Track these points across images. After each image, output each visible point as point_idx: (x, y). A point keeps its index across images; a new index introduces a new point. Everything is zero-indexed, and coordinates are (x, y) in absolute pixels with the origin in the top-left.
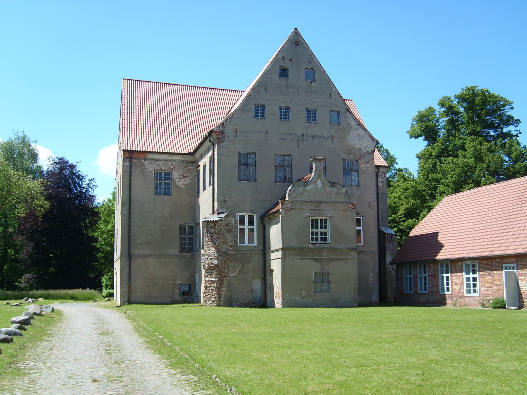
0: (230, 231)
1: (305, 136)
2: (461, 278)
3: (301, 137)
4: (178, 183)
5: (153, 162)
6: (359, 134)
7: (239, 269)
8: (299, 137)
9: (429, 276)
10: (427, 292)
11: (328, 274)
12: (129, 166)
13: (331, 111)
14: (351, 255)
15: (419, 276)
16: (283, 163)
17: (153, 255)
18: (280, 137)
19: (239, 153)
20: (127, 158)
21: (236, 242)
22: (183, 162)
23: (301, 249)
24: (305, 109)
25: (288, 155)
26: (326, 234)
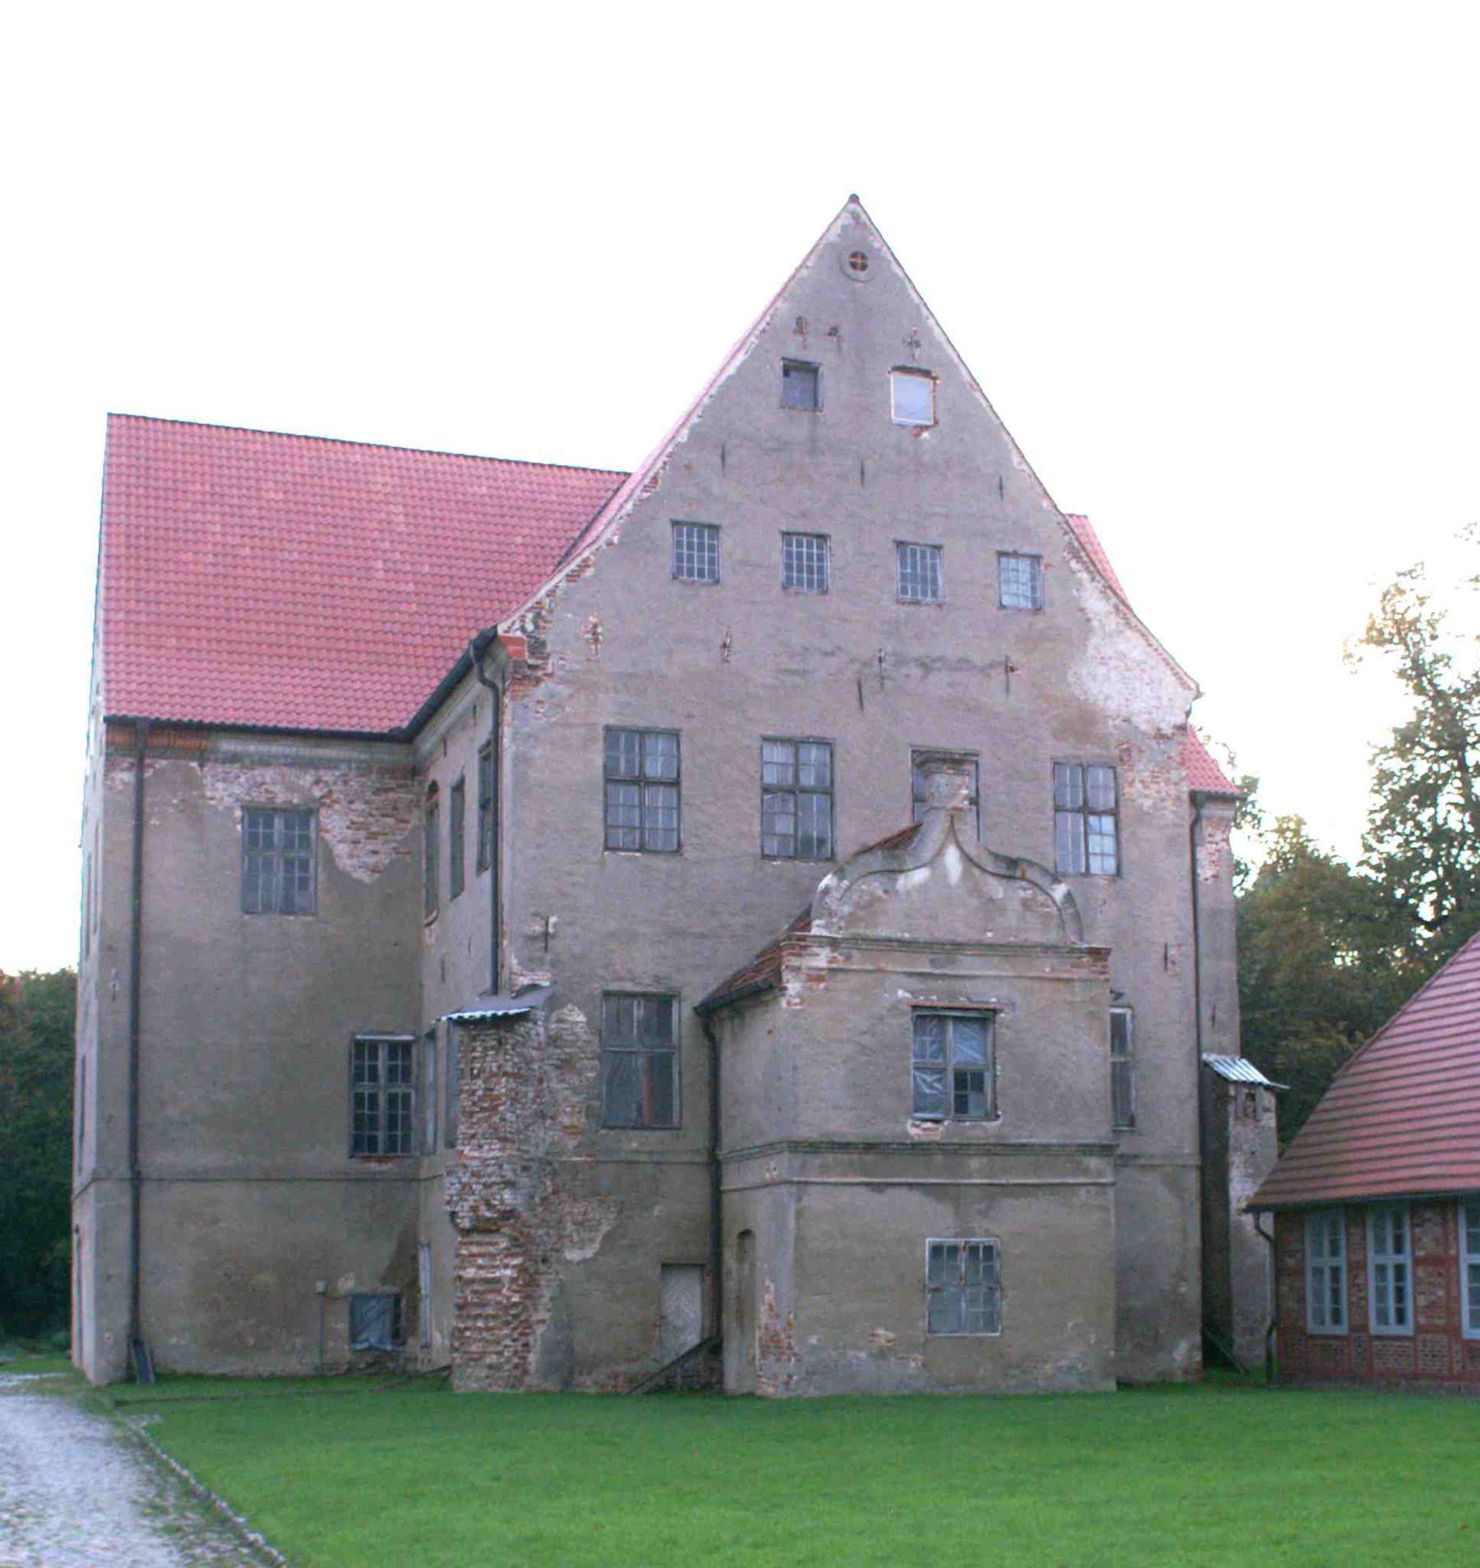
1: (890, 660)
4: (345, 863)
5: (235, 769)
6: (1123, 656)
7: (605, 1228)
8: (865, 664)
9: (1417, 1262)
10: (1408, 1330)
11: (989, 1250)
12: (131, 790)
13: (1002, 554)
15: (1373, 1259)
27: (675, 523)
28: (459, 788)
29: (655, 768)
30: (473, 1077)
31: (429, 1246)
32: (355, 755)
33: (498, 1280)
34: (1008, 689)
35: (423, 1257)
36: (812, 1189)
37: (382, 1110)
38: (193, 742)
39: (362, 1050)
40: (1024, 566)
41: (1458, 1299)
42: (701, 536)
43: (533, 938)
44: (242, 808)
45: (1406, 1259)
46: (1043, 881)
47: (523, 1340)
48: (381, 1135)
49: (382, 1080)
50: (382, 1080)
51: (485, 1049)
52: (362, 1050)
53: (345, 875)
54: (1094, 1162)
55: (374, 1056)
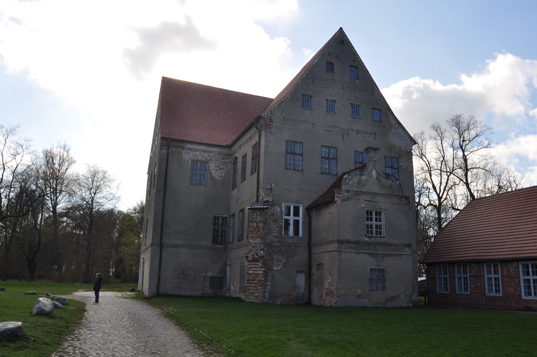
0: (275, 221)
1: (350, 130)
2: (517, 280)
3: (346, 131)
4: (214, 175)
5: (190, 151)
6: (399, 133)
7: (283, 262)
8: (344, 131)
9: (470, 276)
11: (383, 270)
13: (373, 108)
14: (405, 251)
15: (457, 276)
19: (287, 140)
21: (281, 233)
23: (357, 242)
26: (380, 226)
27: (303, 95)
28: (245, 157)
29: (297, 151)
30: (253, 222)
31: (230, 266)
32: (218, 150)
33: (259, 274)
34: (375, 139)
35: (228, 268)
36: (342, 253)
37: (220, 233)
38: (181, 145)
39: (216, 218)
40: (378, 111)
42: (308, 98)
43: (268, 189)
44: (191, 161)
46: (395, 180)
47: (264, 290)
48: (219, 239)
51: (257, 215)
52: (216, 218)
53: (214, 177)
54: (406, 249)
55: (218, 220)
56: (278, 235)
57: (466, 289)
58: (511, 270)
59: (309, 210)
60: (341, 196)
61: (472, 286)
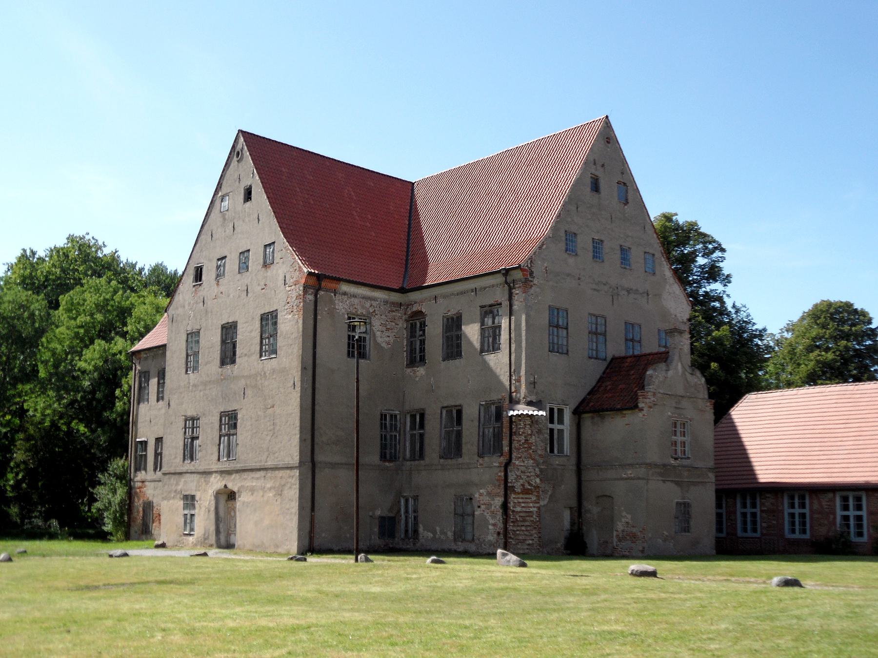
2: (832, 516)
4: (379, 340)
7: (549, 493)
9: (762, 511)
10: (758, 535)
12: (312, 304)
16: (596, 328)
17: (346, 464)
18: (594, 286)
20: (311, 287)
22: (386, 302)
24: (618, 247)
25: (603, 317)
41: (783, 524)
45: (807, 511)
49: (388, 430)
50: (388, 430)
52: (383, 417)
56: (543, 453)
57: (755, 530)
58: (824, 503)
59: (578, 412)
60: (648, 401)
61: (764, 525)
